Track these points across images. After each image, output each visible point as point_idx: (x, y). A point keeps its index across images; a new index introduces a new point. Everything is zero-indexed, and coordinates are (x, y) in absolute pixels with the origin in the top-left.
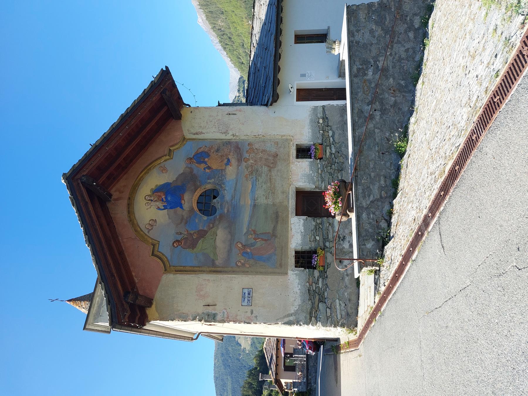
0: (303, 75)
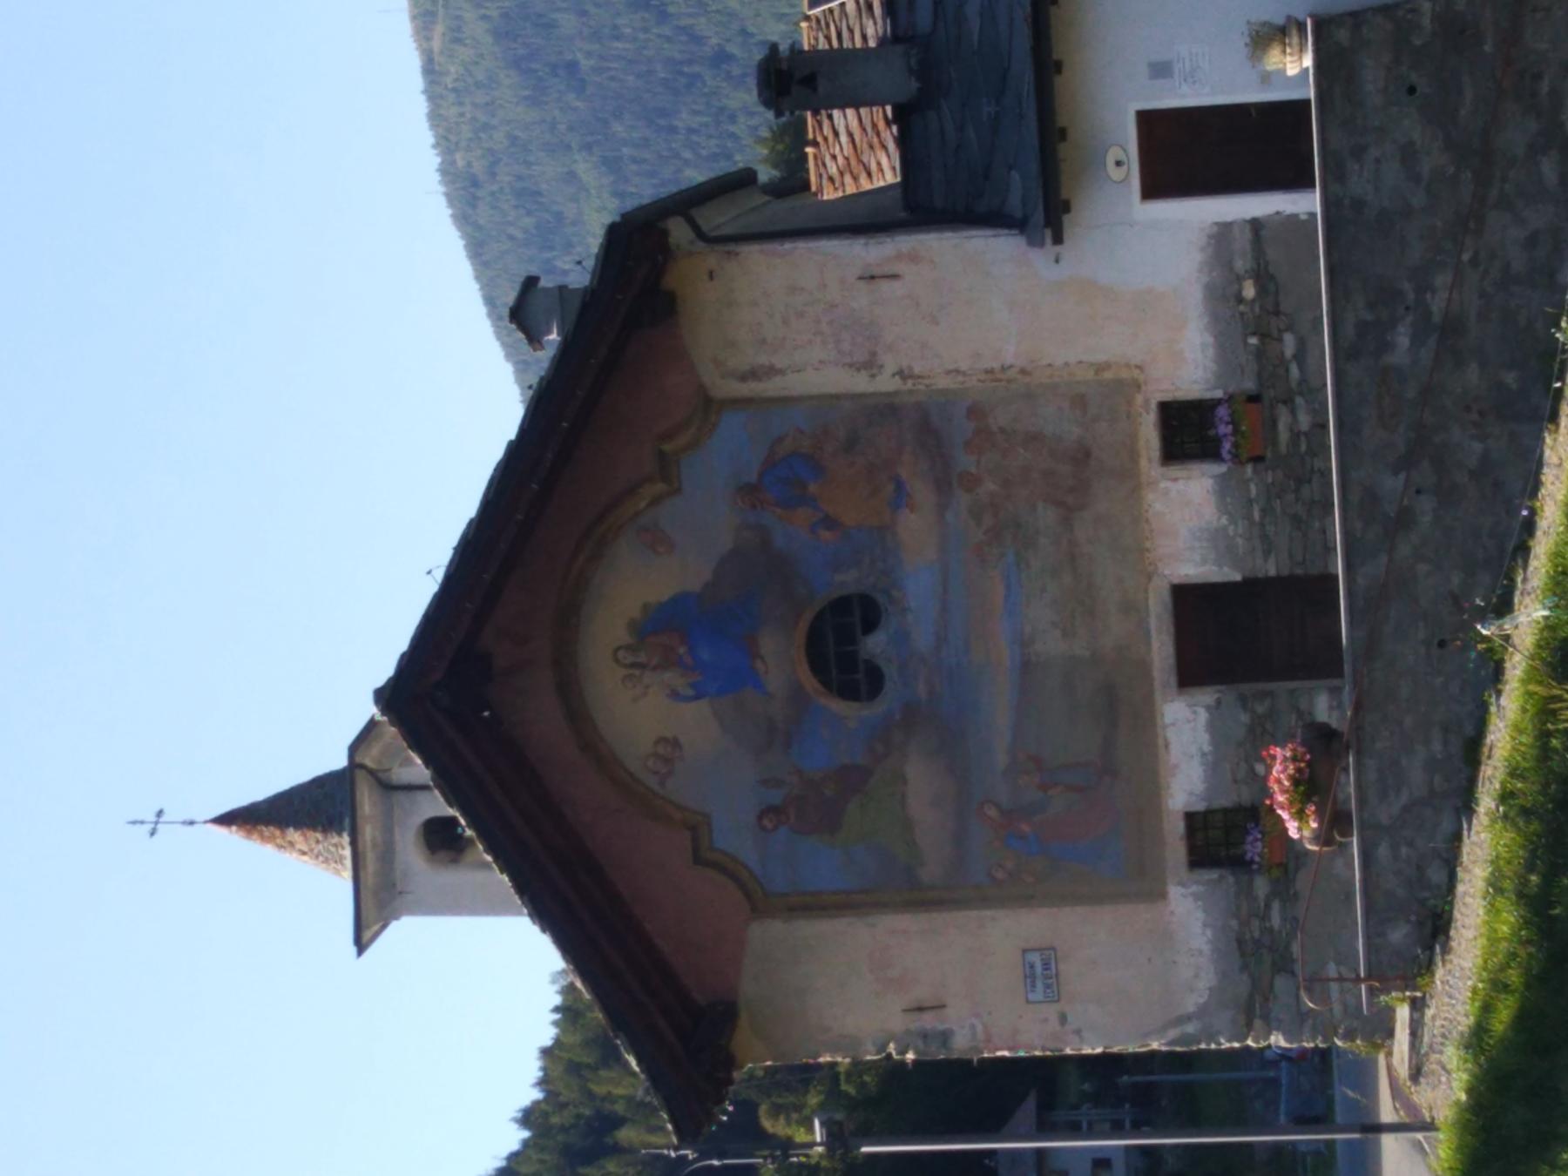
0: (1161, 70)
